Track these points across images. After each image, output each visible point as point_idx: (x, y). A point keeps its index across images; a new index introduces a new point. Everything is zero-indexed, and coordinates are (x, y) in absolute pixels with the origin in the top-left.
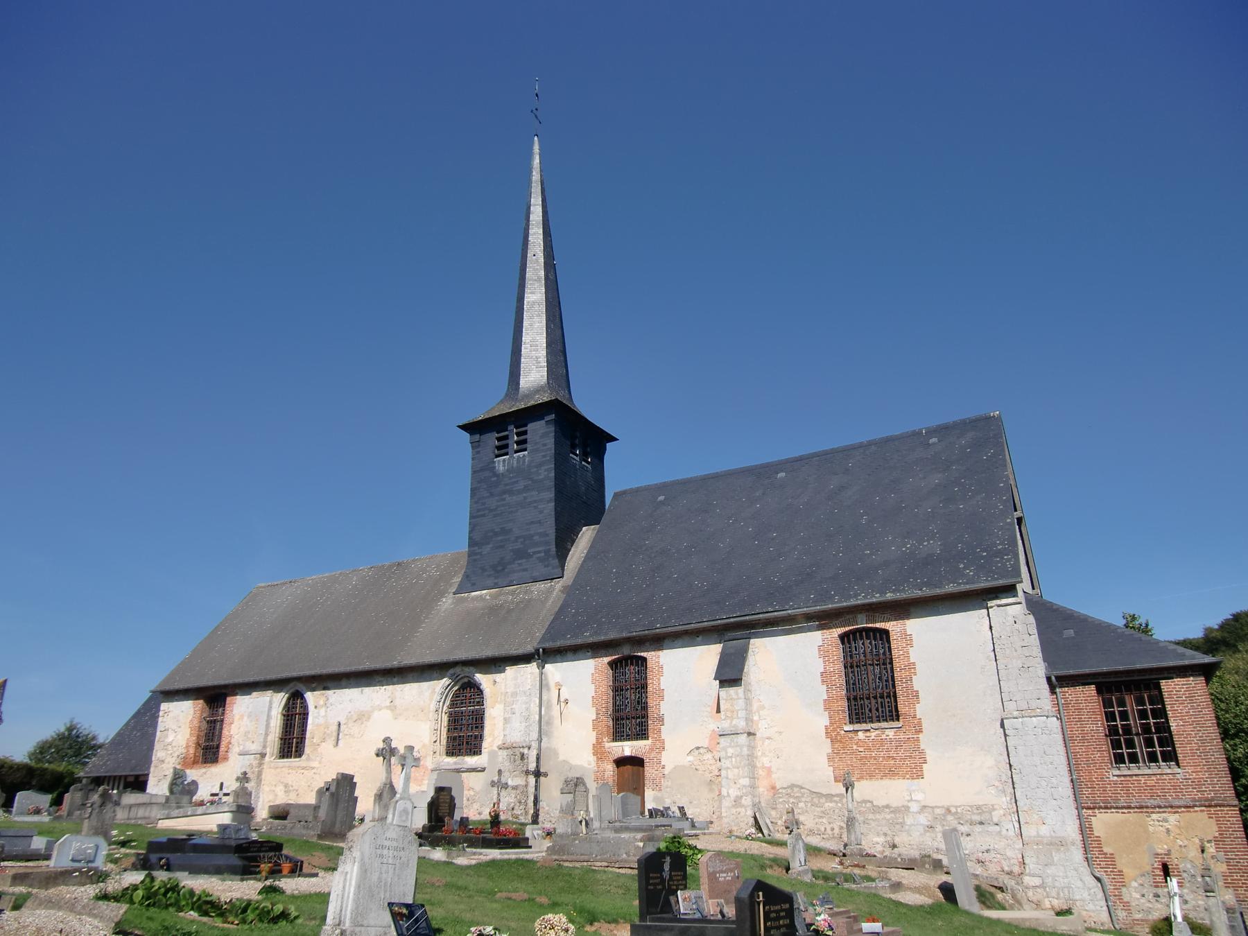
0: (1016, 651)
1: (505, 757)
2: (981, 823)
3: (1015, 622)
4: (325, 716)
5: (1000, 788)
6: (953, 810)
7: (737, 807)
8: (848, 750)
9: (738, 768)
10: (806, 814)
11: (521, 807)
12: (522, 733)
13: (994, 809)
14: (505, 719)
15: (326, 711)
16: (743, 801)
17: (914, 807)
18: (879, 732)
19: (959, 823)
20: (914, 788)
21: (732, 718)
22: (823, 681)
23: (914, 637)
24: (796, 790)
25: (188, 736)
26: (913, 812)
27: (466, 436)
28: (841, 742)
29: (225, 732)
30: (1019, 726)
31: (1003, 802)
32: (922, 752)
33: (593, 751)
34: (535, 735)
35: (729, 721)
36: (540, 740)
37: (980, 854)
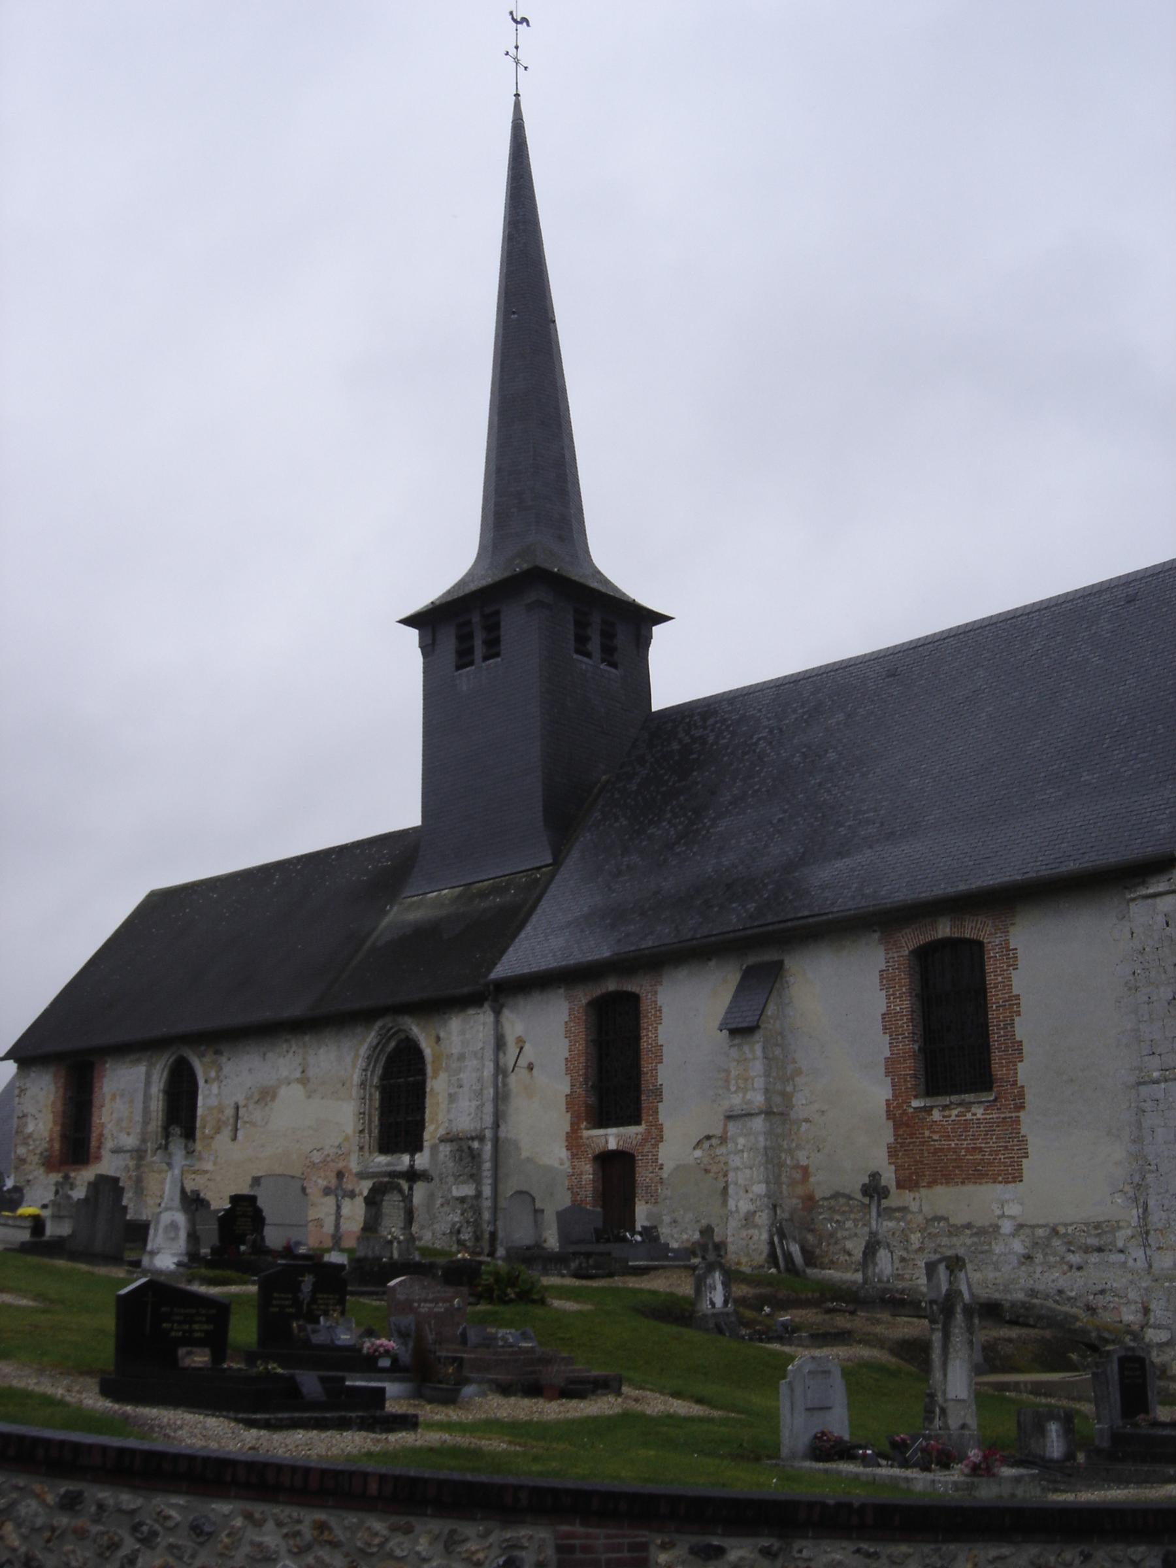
0: (1165, 972)
1: (448, 1153)
2: (1100, 1250)
3: (1168, 925)
4: (219, 1094)
5: (1131, 1194)
6: (1062, 1230)
7: (748, 1229)
8: (917, 1138)
9: (751, 1168)
10: (855, 1238)
11: (469, 1229)
12: (472, 1116)
13: (1119, 1228)
14: (450, 1095)
15: (220, 1087)
16: (757, 1220)
17: (1007, 1227)
18: (962, 1110)
19: (1069, 1251)
20: (1007, 1196)
21: (745, 1090)
22: (885, 1028)
23: (1020, 953)
24: (842, 1201)
25: (50, 1125)
26: (1005, 1235)
27: (413, 634)
28: (907, 1125)
29: (95, 1120)
30: (1160, 1095)
31: (1132, 1217)
32: (1023, 1141)
33: (566, 1144)
34: (488, 1120)
35: (741, 1095)
36: (496, 1126)
37: (1091, 1297)
